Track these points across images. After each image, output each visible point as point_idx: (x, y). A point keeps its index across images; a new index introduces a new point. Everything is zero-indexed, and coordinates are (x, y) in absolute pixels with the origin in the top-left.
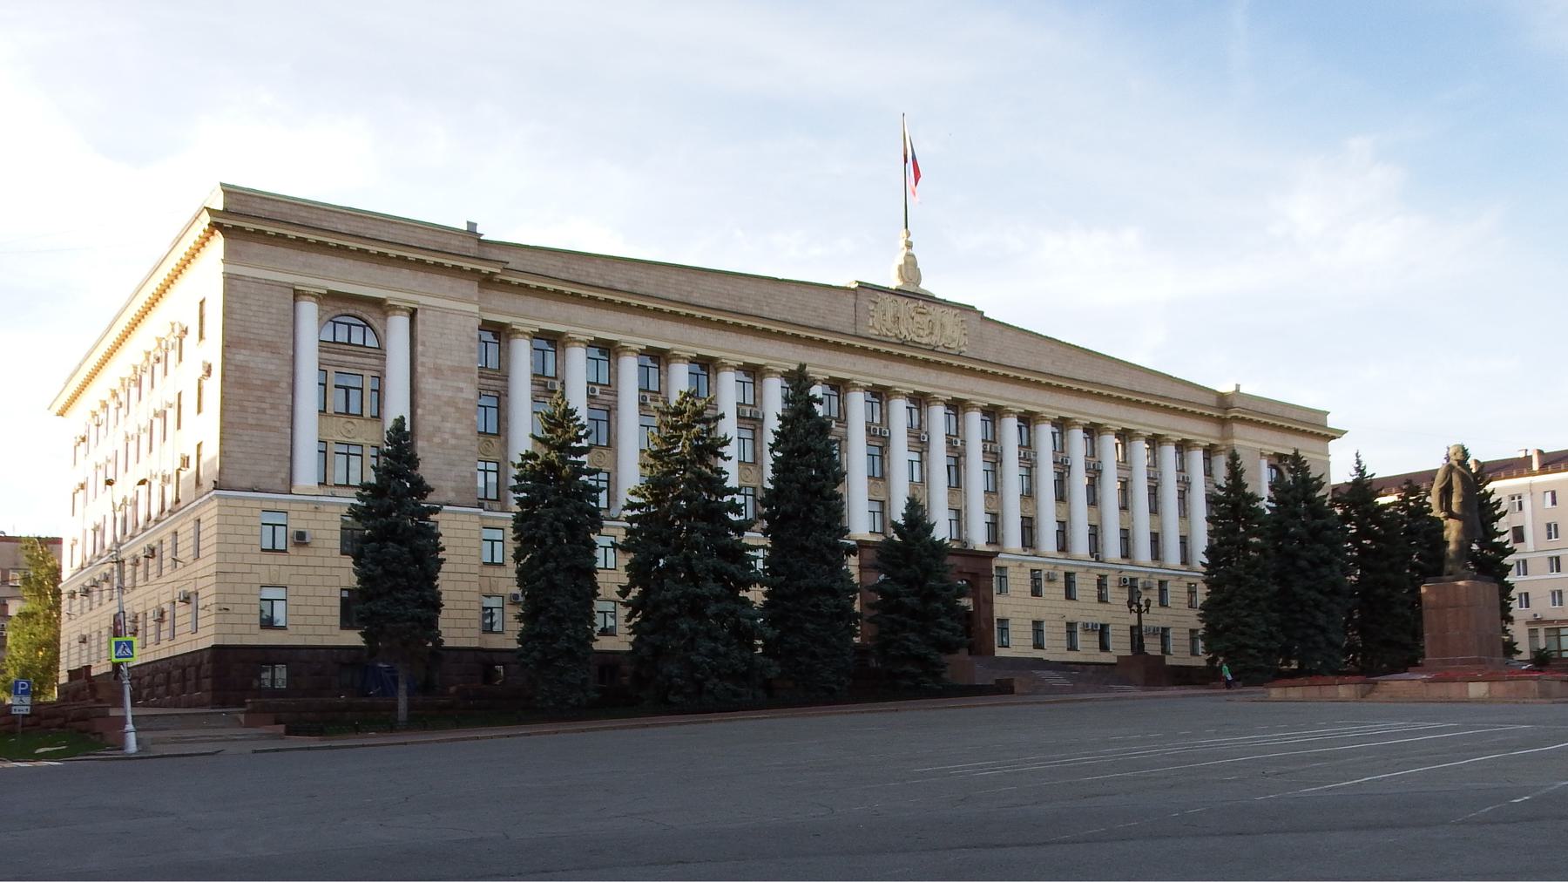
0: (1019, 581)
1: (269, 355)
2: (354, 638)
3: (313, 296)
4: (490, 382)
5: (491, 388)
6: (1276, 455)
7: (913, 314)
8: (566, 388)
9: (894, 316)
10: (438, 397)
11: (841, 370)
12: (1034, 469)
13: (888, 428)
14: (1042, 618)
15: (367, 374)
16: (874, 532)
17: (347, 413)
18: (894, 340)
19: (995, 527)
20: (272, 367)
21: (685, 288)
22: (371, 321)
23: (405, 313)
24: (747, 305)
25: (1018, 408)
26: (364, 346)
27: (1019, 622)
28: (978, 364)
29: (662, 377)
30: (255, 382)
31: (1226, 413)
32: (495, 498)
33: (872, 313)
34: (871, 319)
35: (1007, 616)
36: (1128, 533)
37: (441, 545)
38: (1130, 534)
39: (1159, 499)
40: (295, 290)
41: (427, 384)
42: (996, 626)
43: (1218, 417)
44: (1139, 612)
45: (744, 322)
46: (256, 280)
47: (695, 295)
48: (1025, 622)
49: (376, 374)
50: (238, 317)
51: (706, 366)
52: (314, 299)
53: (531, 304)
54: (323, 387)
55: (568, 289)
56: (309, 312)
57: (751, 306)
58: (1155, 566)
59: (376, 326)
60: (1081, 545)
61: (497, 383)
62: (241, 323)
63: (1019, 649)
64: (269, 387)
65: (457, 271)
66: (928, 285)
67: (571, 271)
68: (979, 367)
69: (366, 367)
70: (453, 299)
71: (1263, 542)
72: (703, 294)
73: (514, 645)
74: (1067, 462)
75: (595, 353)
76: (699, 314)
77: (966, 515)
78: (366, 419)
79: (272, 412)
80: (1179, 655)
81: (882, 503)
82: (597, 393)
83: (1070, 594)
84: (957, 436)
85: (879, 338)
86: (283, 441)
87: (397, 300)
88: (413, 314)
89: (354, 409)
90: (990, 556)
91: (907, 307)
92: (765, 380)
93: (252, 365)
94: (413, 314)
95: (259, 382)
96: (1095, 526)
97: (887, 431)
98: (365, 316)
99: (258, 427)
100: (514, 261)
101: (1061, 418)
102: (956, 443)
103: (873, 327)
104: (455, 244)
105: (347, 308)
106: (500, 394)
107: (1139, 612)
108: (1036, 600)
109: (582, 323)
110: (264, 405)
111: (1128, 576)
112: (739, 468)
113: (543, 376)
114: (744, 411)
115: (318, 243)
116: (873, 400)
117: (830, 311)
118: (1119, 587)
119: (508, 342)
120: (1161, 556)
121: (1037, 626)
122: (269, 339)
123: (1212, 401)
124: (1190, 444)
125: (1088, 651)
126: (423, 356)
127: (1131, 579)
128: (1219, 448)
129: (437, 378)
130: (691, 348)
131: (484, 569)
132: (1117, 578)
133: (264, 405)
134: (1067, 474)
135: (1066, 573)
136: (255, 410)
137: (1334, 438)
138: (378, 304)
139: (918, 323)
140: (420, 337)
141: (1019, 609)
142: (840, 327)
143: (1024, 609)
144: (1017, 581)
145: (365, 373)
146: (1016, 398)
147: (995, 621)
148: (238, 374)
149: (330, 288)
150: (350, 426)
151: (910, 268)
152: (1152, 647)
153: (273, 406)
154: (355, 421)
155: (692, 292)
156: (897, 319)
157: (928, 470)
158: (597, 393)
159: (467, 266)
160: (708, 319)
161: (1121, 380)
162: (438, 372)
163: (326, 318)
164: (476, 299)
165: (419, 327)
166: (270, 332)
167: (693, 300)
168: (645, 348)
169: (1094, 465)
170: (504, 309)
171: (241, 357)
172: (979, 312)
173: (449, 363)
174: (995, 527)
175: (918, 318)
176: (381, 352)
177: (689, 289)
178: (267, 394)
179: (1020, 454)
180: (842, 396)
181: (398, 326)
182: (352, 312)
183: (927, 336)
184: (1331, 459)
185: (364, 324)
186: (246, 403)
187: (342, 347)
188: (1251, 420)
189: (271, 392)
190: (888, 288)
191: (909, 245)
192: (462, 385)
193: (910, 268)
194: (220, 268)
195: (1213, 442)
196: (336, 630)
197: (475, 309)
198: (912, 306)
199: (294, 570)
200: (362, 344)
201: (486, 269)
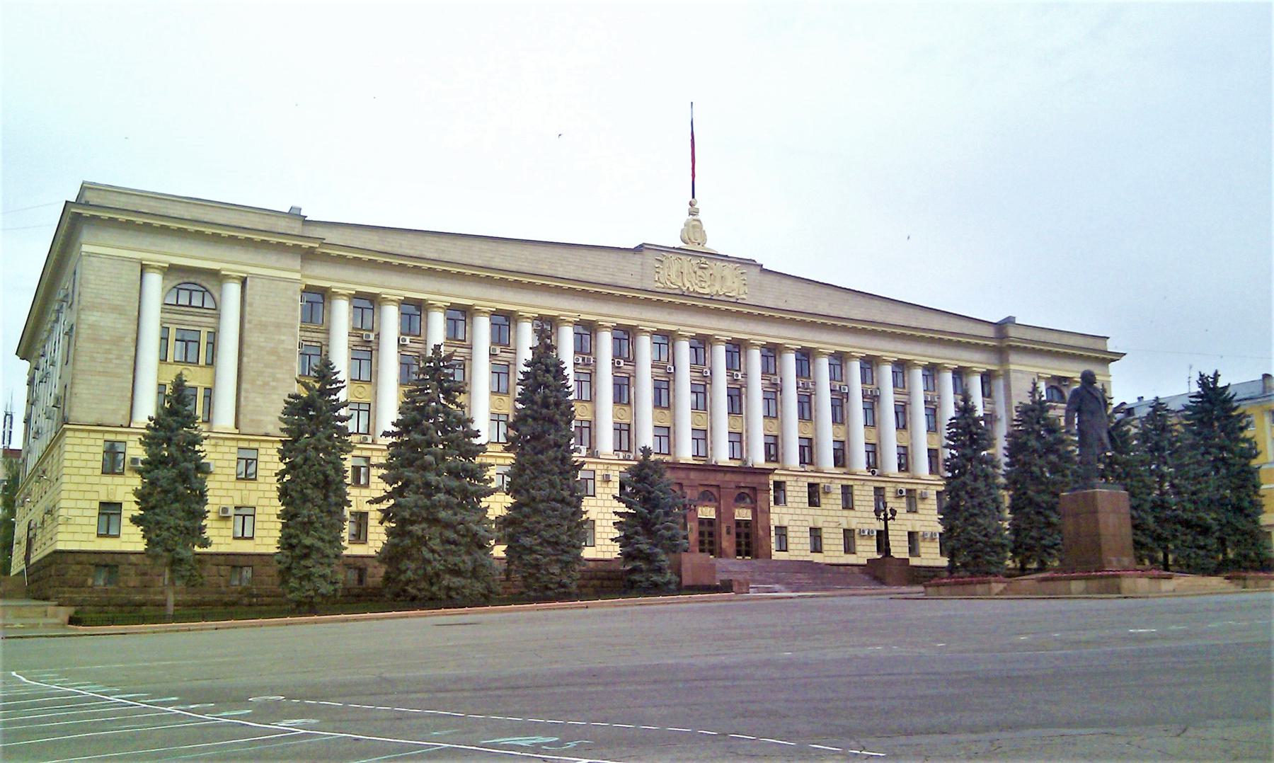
0: (797, 492)
1: (118, 316)
4: (313, 334)
5: (314, 340)
6: (1054, 378)
8: (598, 361)
10: (262, 348)
13: (674, 365)
14: (820, 525)
15: (203, 330)
16: (698, 455)
17: (359, 380)
18: (677, 292)
19: (774, 449)
21: (487, 255)
22: (208, 287)
23: (236, 281)
26: (202, 307)
27: (796, 529)
28: (137, 217)
30: (105, 337)
33: (657, 270)
34: (657, 275)
35: (785, 523)
36: (907, 450)
37: (622, 508)
38: (910, 451)
39: (938, 420)
40: (142, 265)
41: (250, 338)
42: (773, 533)
43: (994, 346)
44: (886, 520)
46: (110, 257)
47: (496, 260)
48: (802, 529)
49: (211, 330)
50: (93, 286)
51: (461, 315)
52: (158, 271)
53: (349, 273)
54: (164, 341)
55: (381, 259)
56: (154, 282)
58: (932, 478)
59: (213, 291)
60: (859, 461)
61: (319, 335)
62: (95, 291)
63: (796, 553)
64: (117, 341)
65: (281, 248)
66: (714, 244)
67: (386, 243)
68: (756, 312)
69: (203, 324)
73: (273, 549)
74: (844, 389)
75: (658, 339)
77: (747, 437)
78: (201, 367)
79: (118, 361)
80: (931, 556)
81: (810, 439)
82: (408, 342)
83: (848, 503)
84: (740, 370)
85: (664, 290)
86: (125, 385)
87: (228, 270)
88: (244, 282)
89: (191, 358)
90: (766, 472)
91: (689, 264)
92: (474, 318)
93: (102, 324)
94: (244, 282)
95: (108, 338)
96: (843, 442)
97: (672, 368)
98: (204, 284)
99: (105, 373)
100: (332, 236)
101: (836, 352)
102: (737, 375)
103: (659, 281)
105: (188, 277)
106: (630, 376)
107: (886, 520)
108: (814, 510)
110: (111, 356)
111: (904, 487)
113: (361, 329)
114: (835, 386)
116: (803, 358)
117: (619, 269)
118: (897, 498)
119: (472, 319)
120: (847, 463)
121: (816, 533)
122: (119, 303)
124: (939, 368)
125: (833, 553)
126: (250, 314)
127: (909, 491)
128: (997, 373)
129: (261, 333)
131: (237, 484)
132: (893, 490)
133: (111, 356)
134: (845, 400)
135: (809, 484)
136: (103, 360)
137: (1114, 361)
138: (215, 275)
140: (248, 299)
141: (795, 517)
142: (480, 262)
143: (802, 518)
144: (795, 494)
145: (203, 330)
147: (773, 528)
148: (90, 332)
150: (360, 389)
151: (694, 227)
152: (899, 549)
153: (119, 357)
154: (192, 368)
157: (711, 399)
158: (408, 342)
159: (290, 242)
162: (263, 327)
163: (169, 287)
164: (299, 268)
165: (248, 291)
166: (120, 298)
167: (493, 265)
169: (871, 391)
170: (321, 276)
171: (94, 318)
172: (758, 265)
173: (273, 320)
174: (774, 449)
175: (700, 272)
176: (217, 313)
177: (491, 255)
178: (114, 347)
179: (797, 383)
180: (631, 340)
181: (232, 292)
182: (192, 280)
183: (709, 286)
184: (1111, 379)
185: (202, 289)
186: (95, 355)
187: (183, 308)
188: (969, 343)
189: (118, 345)
190: (727, 256)
191: (694, 212)
192: (283, 338)
193: (694, 227)
195: (990, 367)
197: (298, 276)
198: (694, 262)
199: (824, 518)
200: (188, 304)
201: (306, 244)
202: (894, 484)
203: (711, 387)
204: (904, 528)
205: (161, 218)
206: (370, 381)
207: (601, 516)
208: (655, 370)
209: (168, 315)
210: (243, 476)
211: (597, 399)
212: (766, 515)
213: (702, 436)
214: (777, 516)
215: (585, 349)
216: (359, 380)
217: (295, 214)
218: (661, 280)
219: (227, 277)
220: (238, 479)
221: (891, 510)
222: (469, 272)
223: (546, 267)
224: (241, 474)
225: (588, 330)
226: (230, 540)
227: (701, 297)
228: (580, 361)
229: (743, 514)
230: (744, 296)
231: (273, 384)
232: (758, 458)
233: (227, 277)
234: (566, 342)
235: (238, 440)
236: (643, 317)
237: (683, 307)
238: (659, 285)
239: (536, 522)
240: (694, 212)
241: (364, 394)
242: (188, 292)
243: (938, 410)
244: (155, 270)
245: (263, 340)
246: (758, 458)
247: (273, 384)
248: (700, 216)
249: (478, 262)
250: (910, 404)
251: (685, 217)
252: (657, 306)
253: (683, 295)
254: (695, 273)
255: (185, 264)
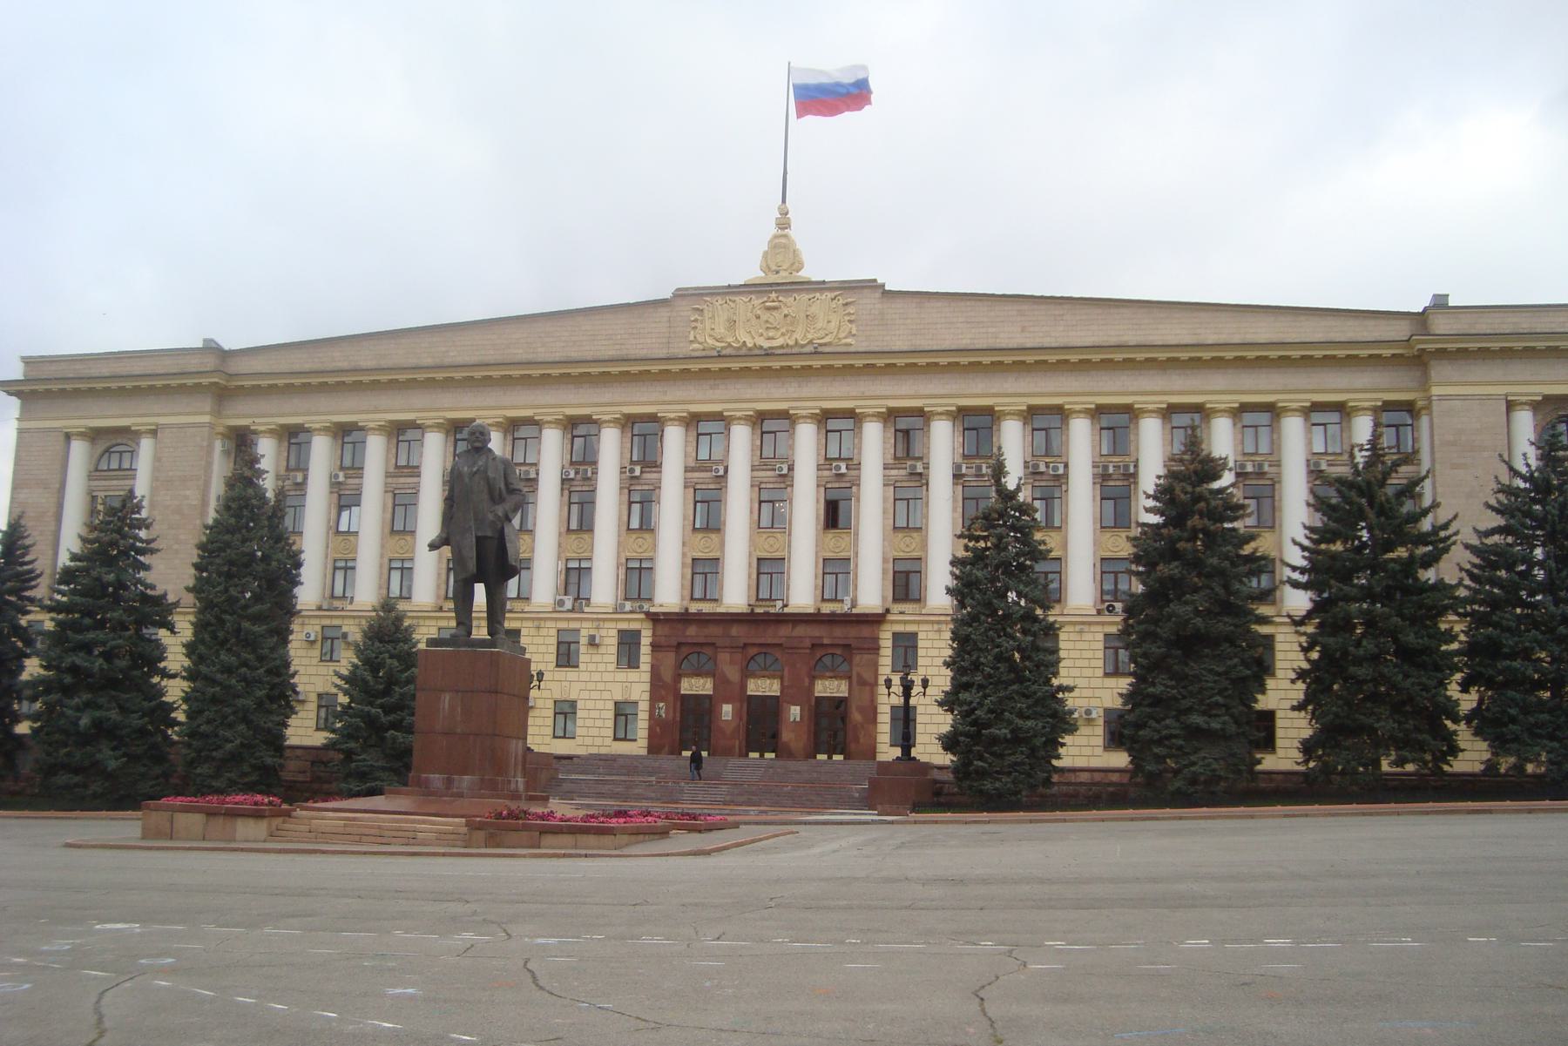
2: (1121, 759)
3: (1013, 414)
7: (759, 312)
9: (728, 320)
11: (467, 409)
12: (1057, 501)
20: (44, 501)
24: (515, 351)
25: (1367, 400)
28: (1182, 352)
29: (1344, 435)
31: (228, 381)
32: (760, 597)
33: (694, 324)
45: (331, 380)
52: (1226, 414)
56: (79, 450)
57: (521, 351)
63: (588, 741)
70: (188, 414)
71: (1503, 594)
72: (520, 348)
76: (129, 385)
85: (704, 354)
87: (1354, 400)
103: (695, 341)
104: (193, 364)
109: (373, 411)
112: (533, 551)
115: (523, 377)
123: (1400, 331)
130: (745, 405)
139: (767, 321)
143: (601, 686)
146: (1157, 389)
149: (824, 407)
150: (771, 541)
155: (447, 351)
156: (732, 323)
158: (843, 470)
160: (1111, 361)
161: (1262, 332)
167: (447, 361)
168: (1025, 408)
175: (765, 316)
177: (444, 349)
190: (824, 282)
192: (188, 493)
194: (14, 424)
196: (1099, 751)
198: (757, 301)
202: (357, 621)
203: (859, 490)
204: (606, 695)
205: (565, 365)
206: (759, 528)
207: (585, 695)
208: (390, 480)
209: (96, 483)
210: (328, 657)
211: (616, 529)
212: (868, 688)
213: (769, 568)
214: (636, 684)
215: (297, 464)
216: (908, 527)
217: (211, 349)
218: (700, 340)
219: (1215, 411)
220: (321, 661)
221: (633, 663)
222: (1364, 353)
223: (521, 351)
224: (326, 654)
225: (294, 437)
226: (548, 739)
227: (768, 354)
228: (572, 475)
229: (829, 688)
230: (849, 340)
231: (176, 547)
232: (870, 593)
233: (1215, 411)
234: (267, 451)
235: (556, 619)
236: (668, 398)
237: (726, 374)
238: (696, 346)
239: (1028, 718)
240: (784, 223)
241: (645, 547)
242: (118, 454)
243: (1277, 486)
244: (871, 418)
245: (168, 498)
246: (870, 593)
247: (176, 547)
248: (792, 233)
249: (428, 361)
250: (1280, 482)
251: (773, 230)
252: (1219, 368)
253: (815, 353)
254: (758, 317)
255: (829, 407)
